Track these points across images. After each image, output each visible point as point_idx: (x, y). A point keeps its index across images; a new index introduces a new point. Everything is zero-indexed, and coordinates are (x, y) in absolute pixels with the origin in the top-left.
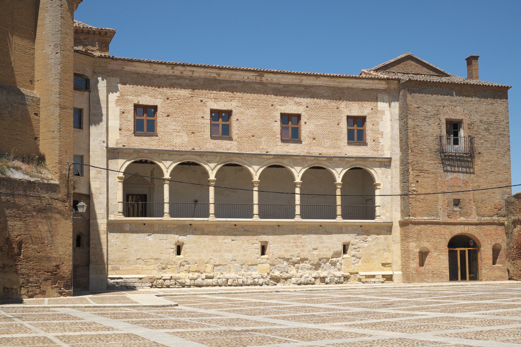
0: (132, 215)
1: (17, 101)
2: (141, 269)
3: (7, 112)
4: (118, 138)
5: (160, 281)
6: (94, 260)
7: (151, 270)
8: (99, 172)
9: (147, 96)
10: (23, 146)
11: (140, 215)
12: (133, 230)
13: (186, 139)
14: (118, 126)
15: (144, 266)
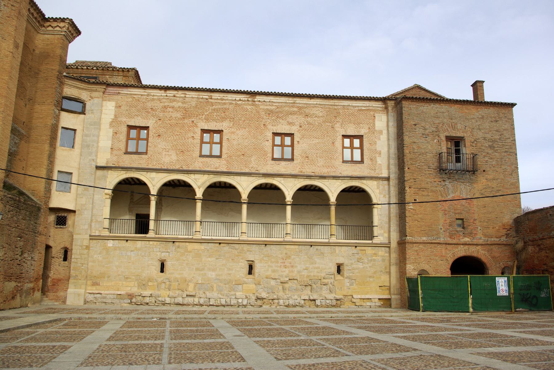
6: (74, 275)
9: (139, 118)
13: (174, 157)
15: (124, 283)
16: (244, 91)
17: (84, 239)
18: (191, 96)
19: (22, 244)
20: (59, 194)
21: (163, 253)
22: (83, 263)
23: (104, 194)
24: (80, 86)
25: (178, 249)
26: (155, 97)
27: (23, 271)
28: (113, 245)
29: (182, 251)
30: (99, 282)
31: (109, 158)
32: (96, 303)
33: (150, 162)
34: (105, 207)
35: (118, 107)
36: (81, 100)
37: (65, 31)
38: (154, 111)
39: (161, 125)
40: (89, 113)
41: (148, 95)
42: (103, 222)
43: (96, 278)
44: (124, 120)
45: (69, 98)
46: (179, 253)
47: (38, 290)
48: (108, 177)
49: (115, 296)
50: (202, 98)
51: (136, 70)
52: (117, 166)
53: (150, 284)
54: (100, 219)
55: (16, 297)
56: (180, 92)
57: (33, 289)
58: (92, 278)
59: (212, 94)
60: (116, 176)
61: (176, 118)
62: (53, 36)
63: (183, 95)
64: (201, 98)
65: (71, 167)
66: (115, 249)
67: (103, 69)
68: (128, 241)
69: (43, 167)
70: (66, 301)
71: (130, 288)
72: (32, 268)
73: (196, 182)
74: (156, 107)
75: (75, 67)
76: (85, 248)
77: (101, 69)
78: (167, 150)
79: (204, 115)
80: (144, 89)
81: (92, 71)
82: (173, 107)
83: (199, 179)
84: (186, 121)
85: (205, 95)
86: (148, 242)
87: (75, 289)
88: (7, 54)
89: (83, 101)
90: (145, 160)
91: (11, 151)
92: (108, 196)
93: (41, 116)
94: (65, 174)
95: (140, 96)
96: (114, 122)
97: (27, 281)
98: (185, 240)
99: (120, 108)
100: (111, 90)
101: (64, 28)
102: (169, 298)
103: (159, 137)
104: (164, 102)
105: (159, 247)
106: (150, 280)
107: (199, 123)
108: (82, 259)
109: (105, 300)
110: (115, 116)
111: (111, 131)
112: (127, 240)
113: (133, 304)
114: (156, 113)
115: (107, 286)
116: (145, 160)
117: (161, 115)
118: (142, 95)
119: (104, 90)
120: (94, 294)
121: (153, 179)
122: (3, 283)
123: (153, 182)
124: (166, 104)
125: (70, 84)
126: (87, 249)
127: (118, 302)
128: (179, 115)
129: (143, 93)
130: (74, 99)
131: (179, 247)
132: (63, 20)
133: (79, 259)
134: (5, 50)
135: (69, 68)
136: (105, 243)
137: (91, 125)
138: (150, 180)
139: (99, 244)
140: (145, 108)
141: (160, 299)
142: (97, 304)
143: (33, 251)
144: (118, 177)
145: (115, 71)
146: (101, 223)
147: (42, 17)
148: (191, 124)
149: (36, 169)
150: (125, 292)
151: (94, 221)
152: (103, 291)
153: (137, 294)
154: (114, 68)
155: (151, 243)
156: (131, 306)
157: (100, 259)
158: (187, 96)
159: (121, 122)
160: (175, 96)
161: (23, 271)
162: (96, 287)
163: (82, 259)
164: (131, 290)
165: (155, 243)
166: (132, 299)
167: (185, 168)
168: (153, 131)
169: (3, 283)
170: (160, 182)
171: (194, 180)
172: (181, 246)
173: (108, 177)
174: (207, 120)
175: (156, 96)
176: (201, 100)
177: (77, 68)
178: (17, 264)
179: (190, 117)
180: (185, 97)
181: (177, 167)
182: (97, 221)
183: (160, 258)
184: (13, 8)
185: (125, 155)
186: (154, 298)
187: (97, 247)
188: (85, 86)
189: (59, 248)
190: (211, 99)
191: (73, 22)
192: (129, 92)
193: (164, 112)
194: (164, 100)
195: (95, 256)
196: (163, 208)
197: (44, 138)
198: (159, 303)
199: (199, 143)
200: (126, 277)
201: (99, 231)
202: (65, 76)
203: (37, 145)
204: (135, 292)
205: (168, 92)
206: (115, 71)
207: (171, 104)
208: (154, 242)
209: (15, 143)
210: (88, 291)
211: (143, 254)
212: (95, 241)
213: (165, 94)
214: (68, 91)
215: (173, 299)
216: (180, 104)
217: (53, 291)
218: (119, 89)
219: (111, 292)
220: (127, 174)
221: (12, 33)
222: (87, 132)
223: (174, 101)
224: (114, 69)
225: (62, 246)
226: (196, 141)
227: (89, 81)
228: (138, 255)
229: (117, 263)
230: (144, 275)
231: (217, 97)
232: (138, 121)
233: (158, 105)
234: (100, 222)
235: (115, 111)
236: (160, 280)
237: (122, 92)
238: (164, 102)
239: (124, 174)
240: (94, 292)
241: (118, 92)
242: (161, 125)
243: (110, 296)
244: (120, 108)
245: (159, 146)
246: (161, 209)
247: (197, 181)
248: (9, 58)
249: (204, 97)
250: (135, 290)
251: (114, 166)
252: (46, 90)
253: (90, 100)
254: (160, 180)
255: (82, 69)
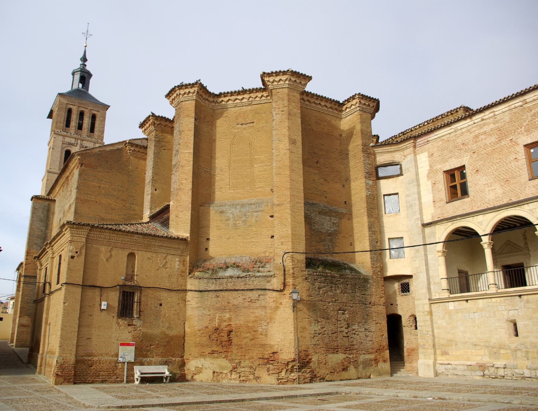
0: (466, 289)
1: (251, 210)
2: (470, 354)
3: (241, 222)
4: (433, 212)
5: (492, 370)
6: (422, 344)
7: (481, 356)
8: (417, 251)
9: (453, 159)
10: (258, 246)
11: (508, 287)
12: (457, 308)
13: (499, 191)
14: (431, 199)
15: (473, 351)
16: (375, 98)
17: (424, 304)
18: (501, 111)
19: (348, 317)
20: (394, 261)
21: (510, 312)
22: (427, 330)
23: (436, 253)
24: (390, 150)
25: (528, 304)
26: (464, 130)
27: (354, 343)
28: (454, 307)
29: (533, 307)
30: (447, 350)
31: (433, 212)
32: (448, 375)
33: (474, 204)
34: (439, 266)
35: (431, 155)
36: (395, 162)
37: (359, 106)
38: (466, 145)
39: (477, 158)
40: (406, 173)
41: (455, 131)
42: (441, 283)
43: (444, 346)
44: (439, 166)
45: (383, 165)
46: (530, 310)
47: (385, 361)
48: (437, 233)
49: (465, 367)
50: (515, 108)
51: (464, 107)
52: (443, 218)
53: (502, 351)
54: (437, 280)
55: (348, 368)
56: (487, 112)
57: (375, 360)
58: (441, 347)
59: (525, 97)
60: (443, 230)
61: (490, 143)
62: (352, 115)
63: (492, 115)
64: (514, 108)
65: (400, 232)
66: (457, 311)
67: (433, 122)
68: (469, 301)
69: (366, 239)
70: (418, 372)
71: (480, 358)
72: (369, 339)
73: (532, 213)
74: (467, 141)
75: (410, 130)
76: (427, 314)
77: (431, 122)
78: (490, 184)
79: (523, 127)
80: (450, 126)
81: (425, 127)
82: (485, 133)
83: (535, 209)
84: (503, 143)
85: (517, 102)
86: (490, 300)
87: (425, 359)
88: (285, 153)
89: (398, 163)
90: (468, 204)
91: (330, 232)
92: (440, 254)
93: (357, 192)
94: (396, 240)
95: (448, 136)
96: (431, 172)
97: (363, 352)
98: (471, 297)
99: (433, 156)
100: (420, 141)
101: (357, 104)
102: (529, 370)
103: (478, 173)
104: (474, 131)
105: (503, 304)
106: (501, 347)
107: (520, 139)
108: (426, 326)
109: (456, 372)
110: (431, 166)
111: (429, 183)
112: (467, 301)
113: (487, 377)
114: (469, 146)
115: (456, 355)
116: (468, 204)
117: (474, 147)
118: (450, 134)
119: (414, 144)
120: (445, 364)
121: (481, 223)
122: (326, 355)
123: (482, 226)
124: (477, 132)
125: (380, 151)
126: (428, 315)
127: (470, 374)
128: (493, 139)
129: (450, 131)
130: (389, 165)
131: (528, 301)
132: (353, 98)
133: (424, 326)
134: (283, 149)
135: (406, 134)
136: (446, 307)
137: (410, 184)
138: (478, 225)
139: (441, 307)
140: (456, 147)
141: (517, 371)
142: (449, 376)
143: (366, 322)
144: (445, 230)
145: (445, 117)
146: (439, 284)
147: (337, 104)
148: (510, 144)
149: (361, 242)
150: (476, 362)
151: (432, 283)
152: (453, 362)
153: (489, 365)
154: (442, 115)
155: (494, 300)
156: (485, 379)
157: (444, 324)
158: (496, 113)
159: (437, 170)
160: (483, 120)
161: (354, 343)
162: (446, 357)
163: (426, 326)
164: (482, 359)
165: (498, 299)
166: (484, 371)
167: (514, 200)
168: (470, 168)
169: (326, 355)
170: (489, 225)
171: (529, 211)
172: (530, 300)
173: (436, 233)
174: (528, 131)
175: (464, 128)
176: (514, 110)
177: (412, 131)
178: (344, 337)
179: (506, 136)
180: (495, 115)
181: (505, 201)
182: (435, 283)
183: (508, 318)
184: (283, 113)
185: (448, 204)
186: (510, 369)
187: (439, 312)
188: (395, 147)
189: (407, 317)
190: (526, 103)
191: (363, 94)
192: (436, 137)
193: (476, 142)
194: (474, 129)
195: (439, 322)
196: (531, 253)
197: (362, 211)
198: (517, 376)
199: (525, 163)
200: (474, 344)
201: (439, 294)
202: (372, 147)
203: (358, 219)
204: (486, 362)
205: (474, 118)
206: (445, 117)
207: (482, 130)
208: (496, 299)
209: (333, 223)
210: (438, 362)
211: (487, 315)
212: (436, 305)
213: (472, 122)
214: (381, 159)
215: (534, 371)
216: (492, 126)
217: (409, 362)
218: (426, 137)
219: (461, 362)
220: (454, 225)
221: (286, 133)
222: (407, 192)
223: (485, 125)
224: (443, 116)
225: (410, 314)
226: (521, 162)
227: (397, 141)
228: (482, 317)
229: (462, 328)
230: (493, 340)
231: (532, 99)
232: (452, 163)
233: (469, 137)
234: (438, 283)
235: (429, 161)
236: (513, 346)
237: (431, 139)
238: (474, 131)
239: (451, 225)
240: (444, 362)
241: (426, 140)
242: (477, 158)
243: (461, 366)
244: (433, 156)
245: (480, 183)
246: (529, 254)
247: (533, 213)
248: (287, 154)
249: (516, 105)
250: (486, 360)
251: (439, 219)
252: (356, 166)
253: (404, 159)
254: (489, 222)
255: (416, 129)
